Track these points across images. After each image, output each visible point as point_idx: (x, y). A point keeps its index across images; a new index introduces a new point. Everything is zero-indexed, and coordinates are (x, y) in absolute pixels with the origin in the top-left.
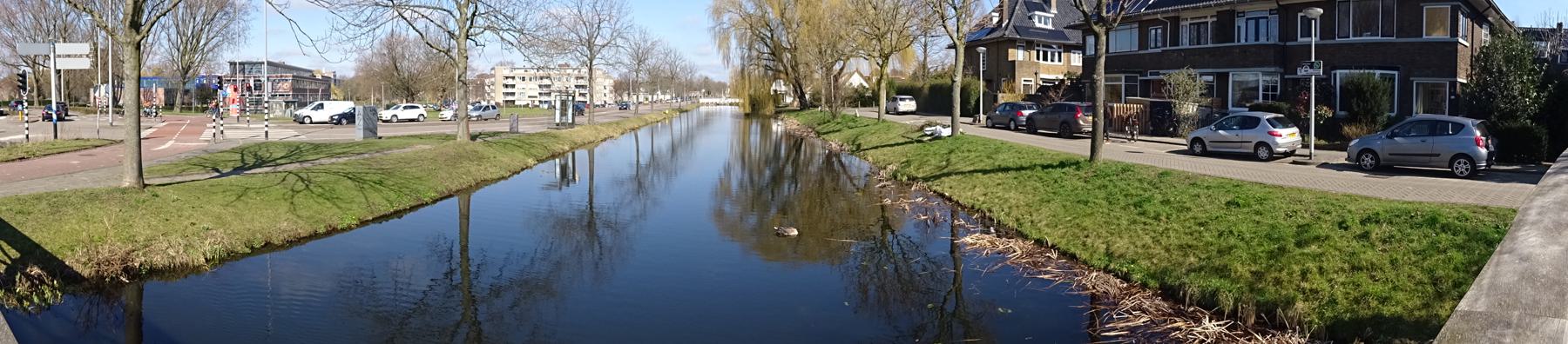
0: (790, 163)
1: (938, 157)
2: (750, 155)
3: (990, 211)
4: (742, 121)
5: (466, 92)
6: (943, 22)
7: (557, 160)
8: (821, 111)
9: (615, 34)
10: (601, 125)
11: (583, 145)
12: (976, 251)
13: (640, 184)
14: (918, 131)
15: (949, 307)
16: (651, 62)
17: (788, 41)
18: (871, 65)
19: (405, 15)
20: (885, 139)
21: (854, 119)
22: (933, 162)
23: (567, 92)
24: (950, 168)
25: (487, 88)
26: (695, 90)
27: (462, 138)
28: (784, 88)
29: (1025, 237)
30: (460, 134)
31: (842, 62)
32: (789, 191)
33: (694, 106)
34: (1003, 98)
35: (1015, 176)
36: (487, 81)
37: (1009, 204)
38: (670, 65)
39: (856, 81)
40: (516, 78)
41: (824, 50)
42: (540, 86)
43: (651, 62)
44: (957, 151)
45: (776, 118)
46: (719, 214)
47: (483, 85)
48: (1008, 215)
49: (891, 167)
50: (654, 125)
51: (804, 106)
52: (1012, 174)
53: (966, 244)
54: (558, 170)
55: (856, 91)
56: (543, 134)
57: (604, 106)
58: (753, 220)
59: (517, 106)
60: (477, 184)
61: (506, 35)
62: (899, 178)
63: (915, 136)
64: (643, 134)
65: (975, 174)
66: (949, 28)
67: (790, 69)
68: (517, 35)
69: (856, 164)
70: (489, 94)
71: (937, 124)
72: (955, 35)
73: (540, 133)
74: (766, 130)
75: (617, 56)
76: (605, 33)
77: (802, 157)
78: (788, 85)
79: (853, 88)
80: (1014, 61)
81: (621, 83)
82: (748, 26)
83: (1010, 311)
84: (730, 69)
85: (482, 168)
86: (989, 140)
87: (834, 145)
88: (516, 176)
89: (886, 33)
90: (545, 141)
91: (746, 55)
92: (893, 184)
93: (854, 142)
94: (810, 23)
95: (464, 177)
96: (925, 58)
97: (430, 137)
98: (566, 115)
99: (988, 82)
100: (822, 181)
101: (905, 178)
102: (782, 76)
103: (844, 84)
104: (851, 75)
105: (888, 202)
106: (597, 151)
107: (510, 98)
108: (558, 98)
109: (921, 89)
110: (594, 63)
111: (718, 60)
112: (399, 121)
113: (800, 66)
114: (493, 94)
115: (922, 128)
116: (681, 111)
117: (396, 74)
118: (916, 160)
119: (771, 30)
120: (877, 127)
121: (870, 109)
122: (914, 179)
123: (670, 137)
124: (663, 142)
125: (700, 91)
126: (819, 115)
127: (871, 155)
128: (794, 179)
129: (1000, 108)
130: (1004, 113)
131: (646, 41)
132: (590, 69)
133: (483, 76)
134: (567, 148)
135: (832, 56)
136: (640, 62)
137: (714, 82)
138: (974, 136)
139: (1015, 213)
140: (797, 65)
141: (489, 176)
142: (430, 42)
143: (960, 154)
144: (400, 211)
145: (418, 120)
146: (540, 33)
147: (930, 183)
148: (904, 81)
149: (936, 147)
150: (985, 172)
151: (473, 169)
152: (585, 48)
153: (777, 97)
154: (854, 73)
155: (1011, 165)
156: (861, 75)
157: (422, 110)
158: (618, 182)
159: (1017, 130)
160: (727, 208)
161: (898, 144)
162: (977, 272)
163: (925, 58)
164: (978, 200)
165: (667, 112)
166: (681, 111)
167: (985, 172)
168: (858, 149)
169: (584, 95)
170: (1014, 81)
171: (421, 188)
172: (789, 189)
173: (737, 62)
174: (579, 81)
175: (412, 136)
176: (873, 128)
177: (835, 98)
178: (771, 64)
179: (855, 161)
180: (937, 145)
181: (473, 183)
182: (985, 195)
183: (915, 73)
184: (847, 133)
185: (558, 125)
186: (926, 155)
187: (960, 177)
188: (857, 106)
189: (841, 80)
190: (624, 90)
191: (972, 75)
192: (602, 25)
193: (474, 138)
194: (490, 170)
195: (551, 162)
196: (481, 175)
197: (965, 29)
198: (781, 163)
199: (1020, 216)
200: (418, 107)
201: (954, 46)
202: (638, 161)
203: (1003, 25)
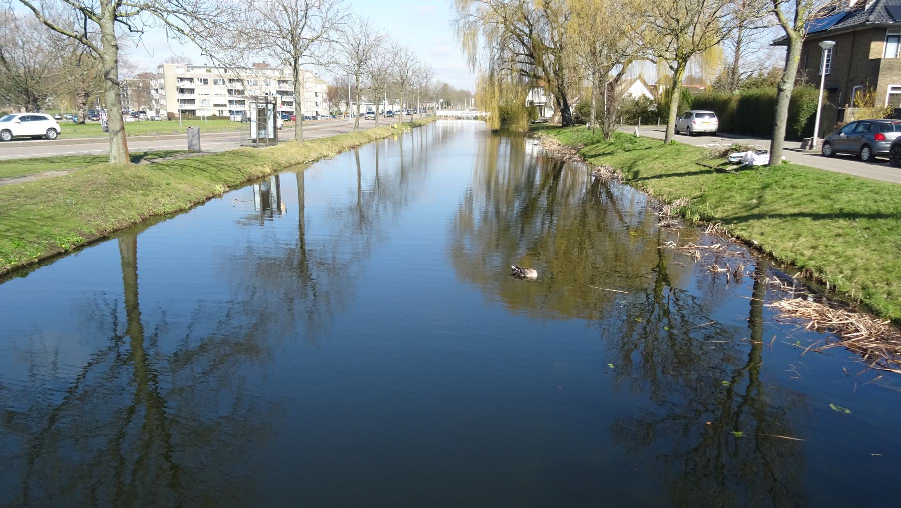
0: (546, 191)
1: (746, 193)
2: (497, 181)
3: (821, 271)
4: (489, 140)
5: (118, 95)
6: (776, 7)
7: (257, 187)
8: (589, 128)
9: (327, 25)
10: (313, 141)
11: (289, 167)
12: (795, 321)
13: (362, 217)
14: (720, 157)
15: (741, 388)
16: (375, 63)
17: (552, 38)
18: (658, 70)
20: (672, 166)
21: (632, 139)
22: (738, 198)
23: (266, 99)
24: (763, 209)
25: (153, 92)
26: (432, 99)
27: (117, 158)
28: (543, 99)
29: (875, 313)
30: (114, 153)
31: (621, 66)
32: (542, 228)
33: (430, 119)
34: (852, 115)
35: (867, 226)
36: (153, 83)
37: (853, 265)
38: (400, 67)
39: (638, 92)
40: (195, 80)
41: (598, 49)
42: (230, 91)
43: (375, 63)
44: (774, 186)
45: (530, 137)
46: (457, 252)
47: (147, 88)
48: (850, 279)
49: (681, 203)
50: (380, 141)
51: (567, 122)
52: (862, 223)
53: (781, 311)
54: (258, 199)
55: (637, 103)
56: (235, 154)
57: (315, 118)
58: (497, 260)
59: (199, 118)
60: (144, 220)
61: (172, 18)
62: (688, 217)
63: (715, 163)
64: (366, 154)
65: (801, 219)
66: (783, 17)
67: (552, 75)
68: (188, 19)
69: (629, 197)
70: (157, 101)
71: (747, 149)
72: (791, 25)
73: (230, 152)
74: (517, 152)
75: (331, 53)
76: (314, 22)
77: (561, 183)
78: (549, 95)
79: (634, 100)
80: (878, 61)
81: (337, 89)
82: (501, 19)
83: (848, 411)
84: (476, 74)
85: (151, 198)
86: (826, 173)
87: (603, 171)
88: (199, 208)
89: (687, 26)
90: (238, 161)
91: (497, 57)
92: (680, 224)
93: (630, 168)
94: (582, 15)
95: (123, 211)
96: (737, 60)
97: (66, 159)
98: (265, 128)
99: (832, 91)
100: (584, 215)
101: (696, 218)
102: (542, 83)
103: (621, 94)
104: (632, 82)
105: (672, 245)
106: (308, 174)
107: (188, 107)
108: (253, 106)
109: (726, 102)
110: (300, 61)
111: (459, 59)
112: (14, 139)
113: (565, 71)
114: (162, 101)
115: (725, 154)
116: (414, 125)
118: (714, 195)
119: (530, 25)
120: (662, 151)
121: (654, 127)
122: (707, 220)
123: (400, 159)
124: (390, 164)
125: (438, 101)
126: (586, 134)
127: (653, 186)
128: (550, 211)
129: (847, 129)
130: (852, 137)
131: (368, 35)
132: (296, 69)
133: (146, 76)
134: (268, 170)
135: (608, 58)
136: (361, 62)
137: (455, 91)
138: (804, 167)
139: (861, 277)
140: (561, 69)
141: (160, 210)
142: (49, 22)
143: (779, 191)
144: (23, 267)
145: (46, 137)
146: (223, 18)
147: (732, 226)
148: (705, 89)
149: (746, 179)
150: (816, 217)
151: (137, 201)
152: (288, 42)
153: (532, 110)
154: (635, 80)
155: (860, 209)
156: (645, 84)
157: (51, 122)
158: (334, 213)
159: (872, 160)
160: (467, 243)
161: (690, 174)
162: (796, 348)
163: (737, 60)
164: (802, 254)
165: (396, 126)
166: (414, 125)
167: (816, 217)
168: (634, 178)
169: (290, 104)
170: (875, 89)
171: (53, 231)
172: (543, 224)
173: (484, 65)
175: (36, 160)
176: (658, 152)
177: (609, 113)
178: (527, 68)
179: (628, 191)
180: (745, 177)
181: (138, 220)
182: (814, 248)
183: (719, 80)
184: (622, 157)
185: (254, 141)
186: (729, 190)
187: (777, 221)
188: (636, 124)
189: (618, 89)
190: (342, 98)
191: (807, 82)
192: (310, 12)
193: (136, 159)
194: (162, 201)
195: (247, 189)
196: (147, 211)
197: (804, 15)
198: (534, 193)
199: (870, 284)
200: (44, 118)
201: (787, 41)
202: (360, 185)
203: (867, 7)
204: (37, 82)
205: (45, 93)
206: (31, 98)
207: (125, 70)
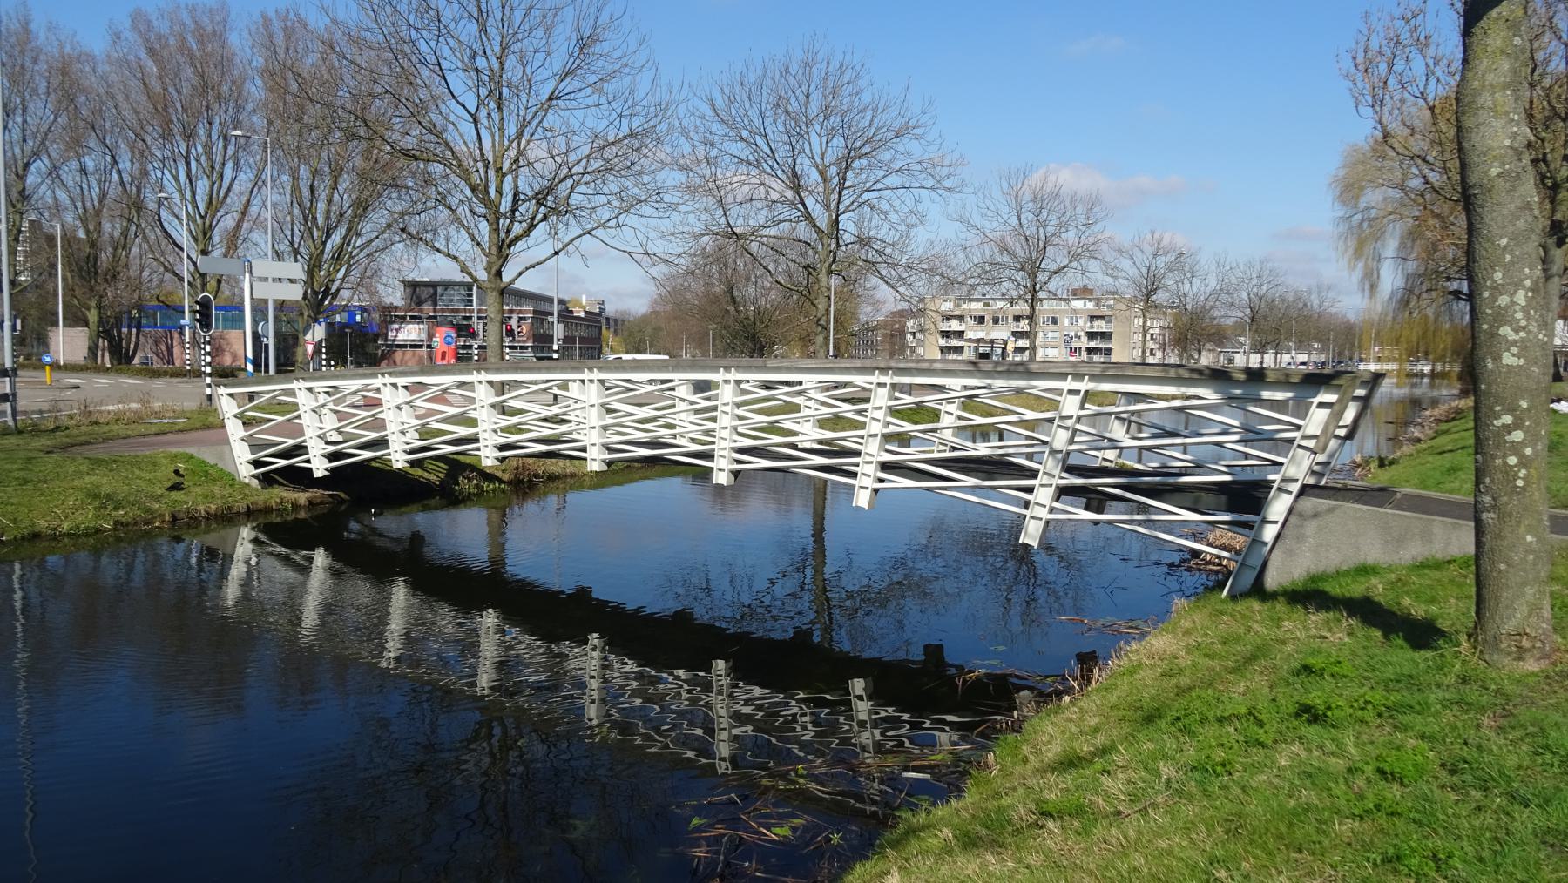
19: (787, 224)
25: (909, 336)
47: (902, 333)
117: (732, 309)
159: (14, 356)
174: (1096, 323)
204: (767, 326)
205: (773, 339)
206: (758, 345)
207: (869, 309)
